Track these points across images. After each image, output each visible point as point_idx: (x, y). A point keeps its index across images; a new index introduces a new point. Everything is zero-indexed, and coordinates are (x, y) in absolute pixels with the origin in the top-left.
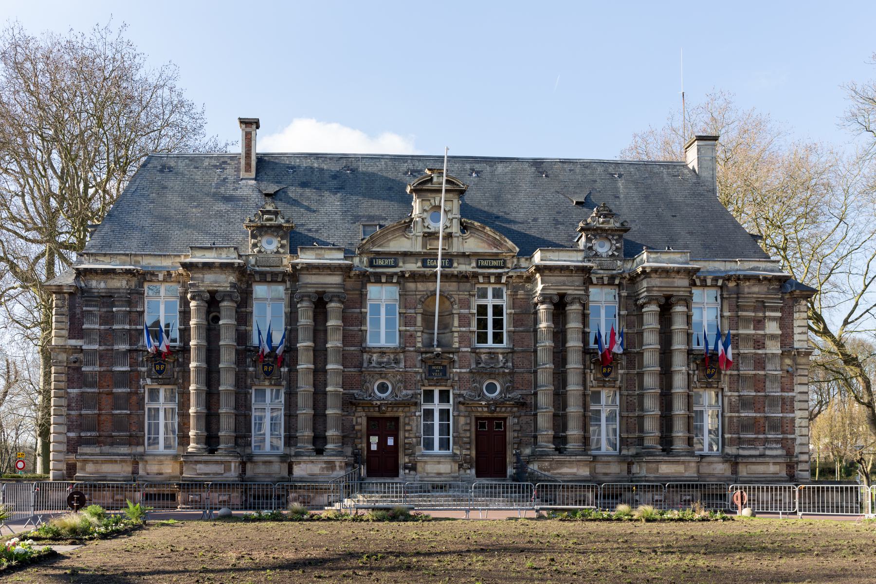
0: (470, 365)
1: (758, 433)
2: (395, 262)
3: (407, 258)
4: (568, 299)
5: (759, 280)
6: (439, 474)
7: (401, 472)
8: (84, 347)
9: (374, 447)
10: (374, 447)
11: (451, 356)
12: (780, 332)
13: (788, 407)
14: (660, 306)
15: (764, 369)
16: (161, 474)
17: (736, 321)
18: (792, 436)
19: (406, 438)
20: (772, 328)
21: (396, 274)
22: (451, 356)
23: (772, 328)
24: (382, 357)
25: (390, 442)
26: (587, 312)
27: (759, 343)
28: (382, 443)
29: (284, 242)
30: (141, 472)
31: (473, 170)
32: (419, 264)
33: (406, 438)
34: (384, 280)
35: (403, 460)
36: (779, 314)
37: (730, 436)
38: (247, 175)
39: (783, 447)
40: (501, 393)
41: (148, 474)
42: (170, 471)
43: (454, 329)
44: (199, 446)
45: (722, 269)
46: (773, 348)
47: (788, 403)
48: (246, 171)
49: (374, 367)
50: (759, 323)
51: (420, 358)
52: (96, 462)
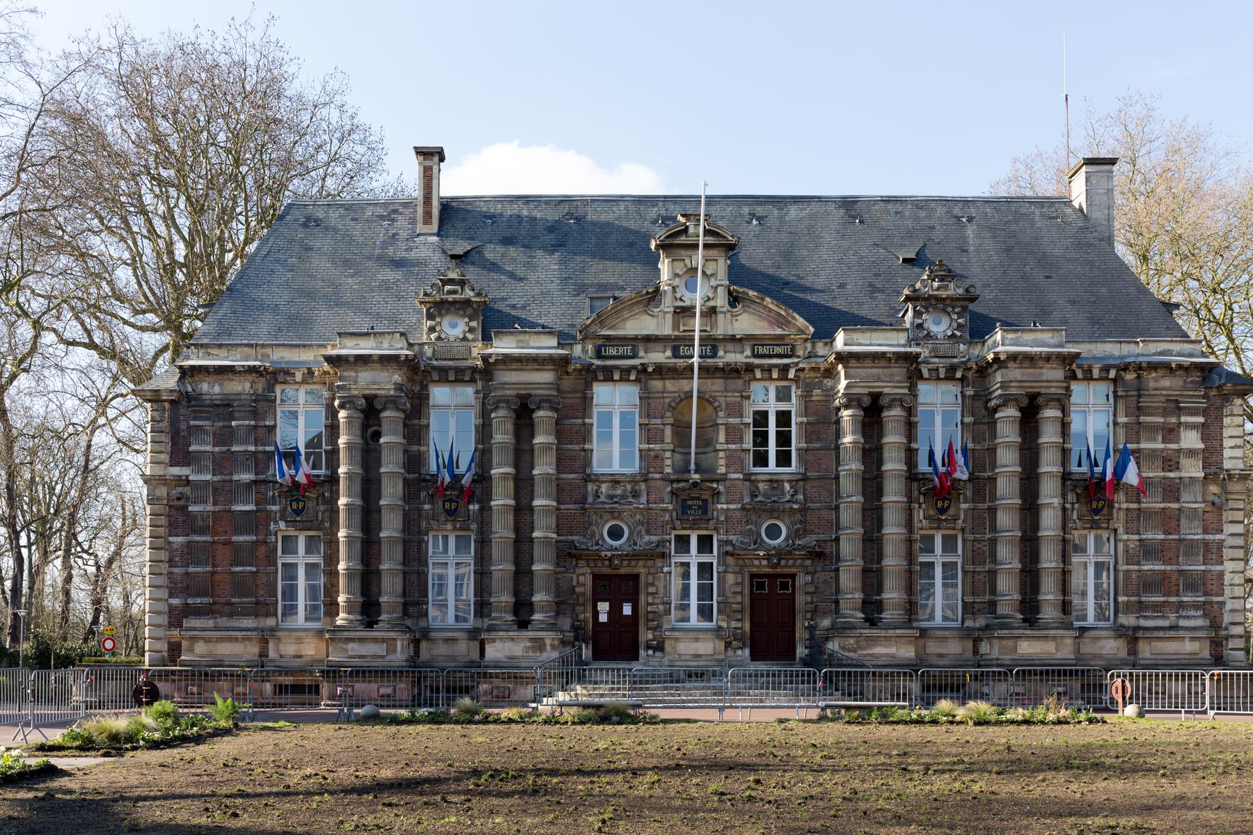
0: (742, 498)
1: (1169, 594)
2: (633, 350)
4: (884, 401)
5: (1171, 369)
6: (697, 656)
7: (642, 653)
8: (191, 478)
9: (603, 618)
10: (603, 618)
11: (715, 485)
12: (1202, 446)
13: (1214, 556)
14: (1021, 410)
15: (1178, 500)
16: (300, 657)
17: (1136, 430)
18: (1220, 599)
19: (648, 604)
20: (1191, 440)
21: (634, 367)
22: (715, 485)
23: (1191, 440)
24: (614, 488)
27: (1170, 462)
28: (615, 611)
29: (474, 324)
32: (669, 353)
33: (648, 604)
34: (616, 377)
35: (646, 635)
36: (1201, 420)
37: (1125, 599)
38: (426, 229)
39: (1205, 615)
40: (787, 539)
41: (281, 656)
45: (1116, 354)
47: (1214, 550)
48: (425, 223)
49: (603, 503)
50: (1171, 433)
51: (669, 489)
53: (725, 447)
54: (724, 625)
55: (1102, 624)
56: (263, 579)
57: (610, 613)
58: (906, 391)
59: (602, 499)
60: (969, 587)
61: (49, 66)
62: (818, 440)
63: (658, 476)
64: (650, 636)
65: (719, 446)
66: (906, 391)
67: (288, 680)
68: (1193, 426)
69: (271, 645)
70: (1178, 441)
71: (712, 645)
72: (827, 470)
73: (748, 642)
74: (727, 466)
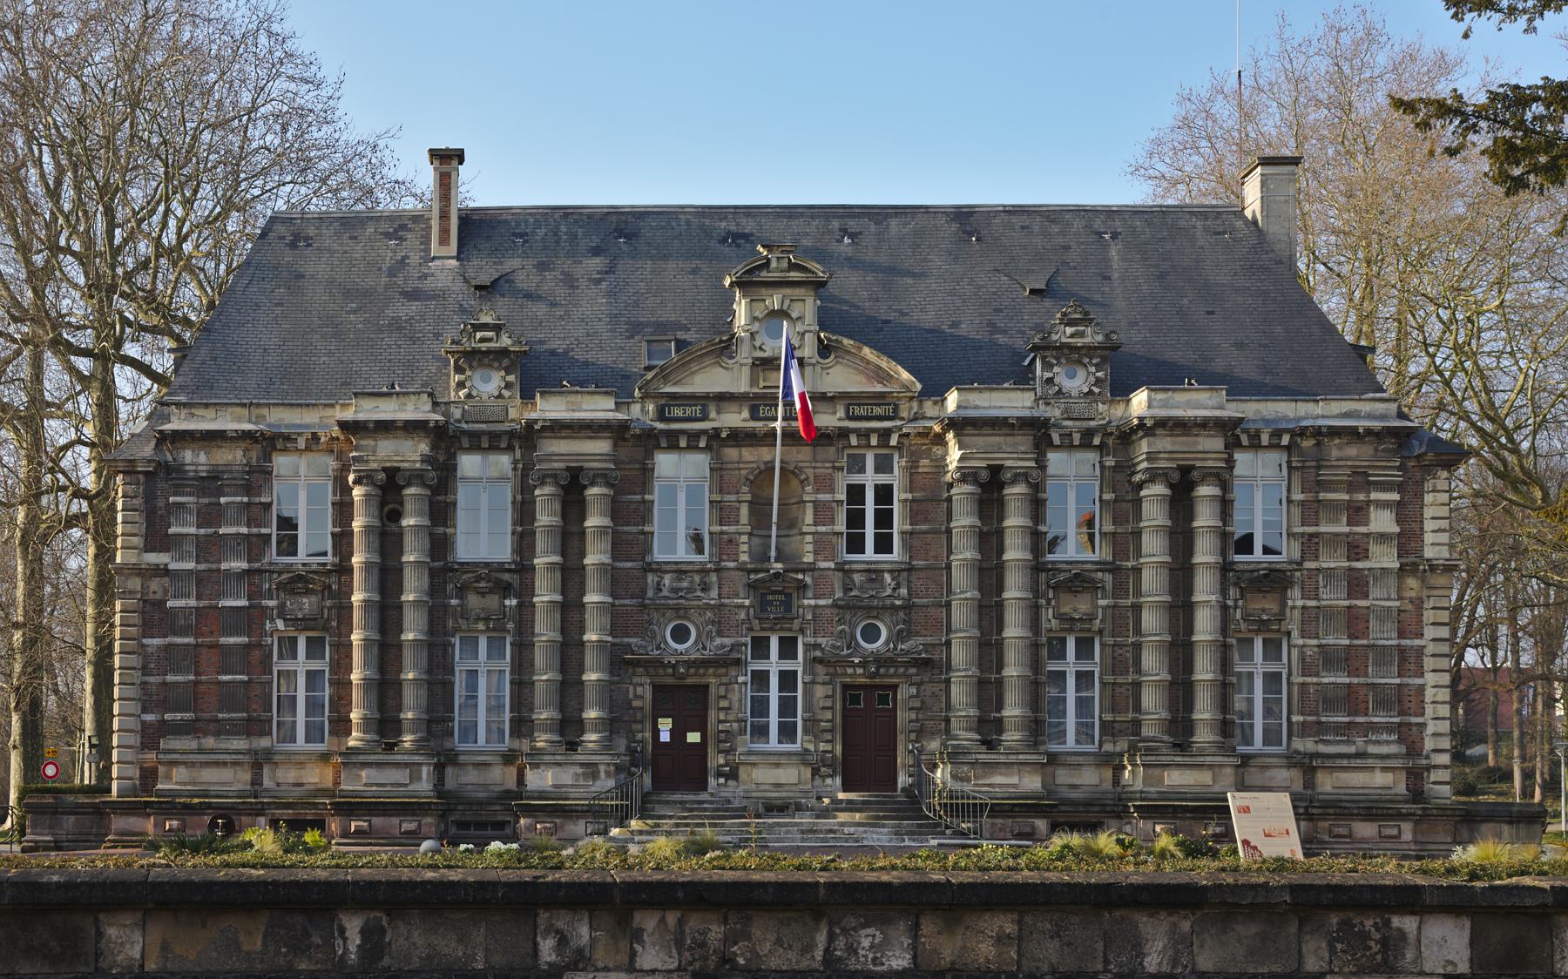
1: (1356, 714)
11: (800, 576)
13: (1412, 667)
14: (1171, 486)
15: (1366, 597)
18: (1420, 720)
21: (704, 432)
22: (800, 576)
26: (1230, 496)
27: (1356, 549)
29: (511, 378)
31: (844, 232)
32: (746, 414)
36: (1395, 496)
38: (444, 251)
39: (1400, 741)
40: (887, 642)
51: (745, 580)
53: (813, 529)
54: (811, 747)
58: (1032, 464)
59: (665, 593)
60: (1108, 702)
62: (926, 521)
63: (731, 565)
64: (722, 761)
65: (805, 529)
66: (1032, 464)
72: (936, 557)
73: (839, 769)
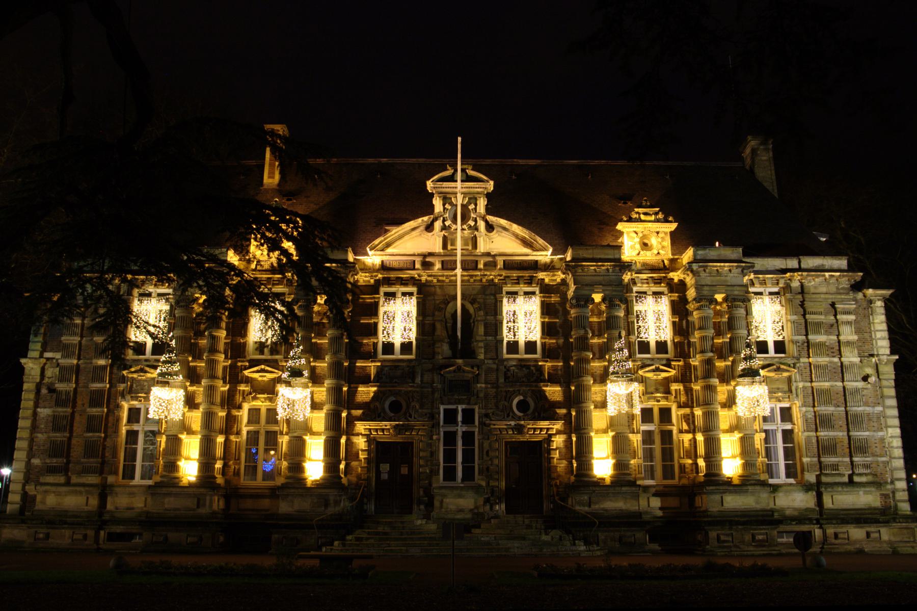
3: (836, 488)
6: (461, 511)
8: (60, 361)
9: (385, 476)
10: (385, 476)
12: (855, 337)
16: (132, 508)
17: (806, 328)
19: (421, 466)
20: (848, 334)
23: (848, 334)
24: (61, 380)
25: (404, 470)
28: (393, 471)
30: (109, 506)
33: (421, 466)
37: (809, 459)
41: (117, 508)
42: (141, 505)
43: (478, 338)
44: (795, 317)
46: (851, 357)
47: (875, 420)
50: (834, 327)
52: (58, 494)
55: (792, 481)
56: (109, 443)
57: (389, 473)
61: (528, 324)
67: (119, 529)
68: (849, 323)
69: (109, 499)
70: (49, 437)
71: (473, 501)
74: (485, 353)
